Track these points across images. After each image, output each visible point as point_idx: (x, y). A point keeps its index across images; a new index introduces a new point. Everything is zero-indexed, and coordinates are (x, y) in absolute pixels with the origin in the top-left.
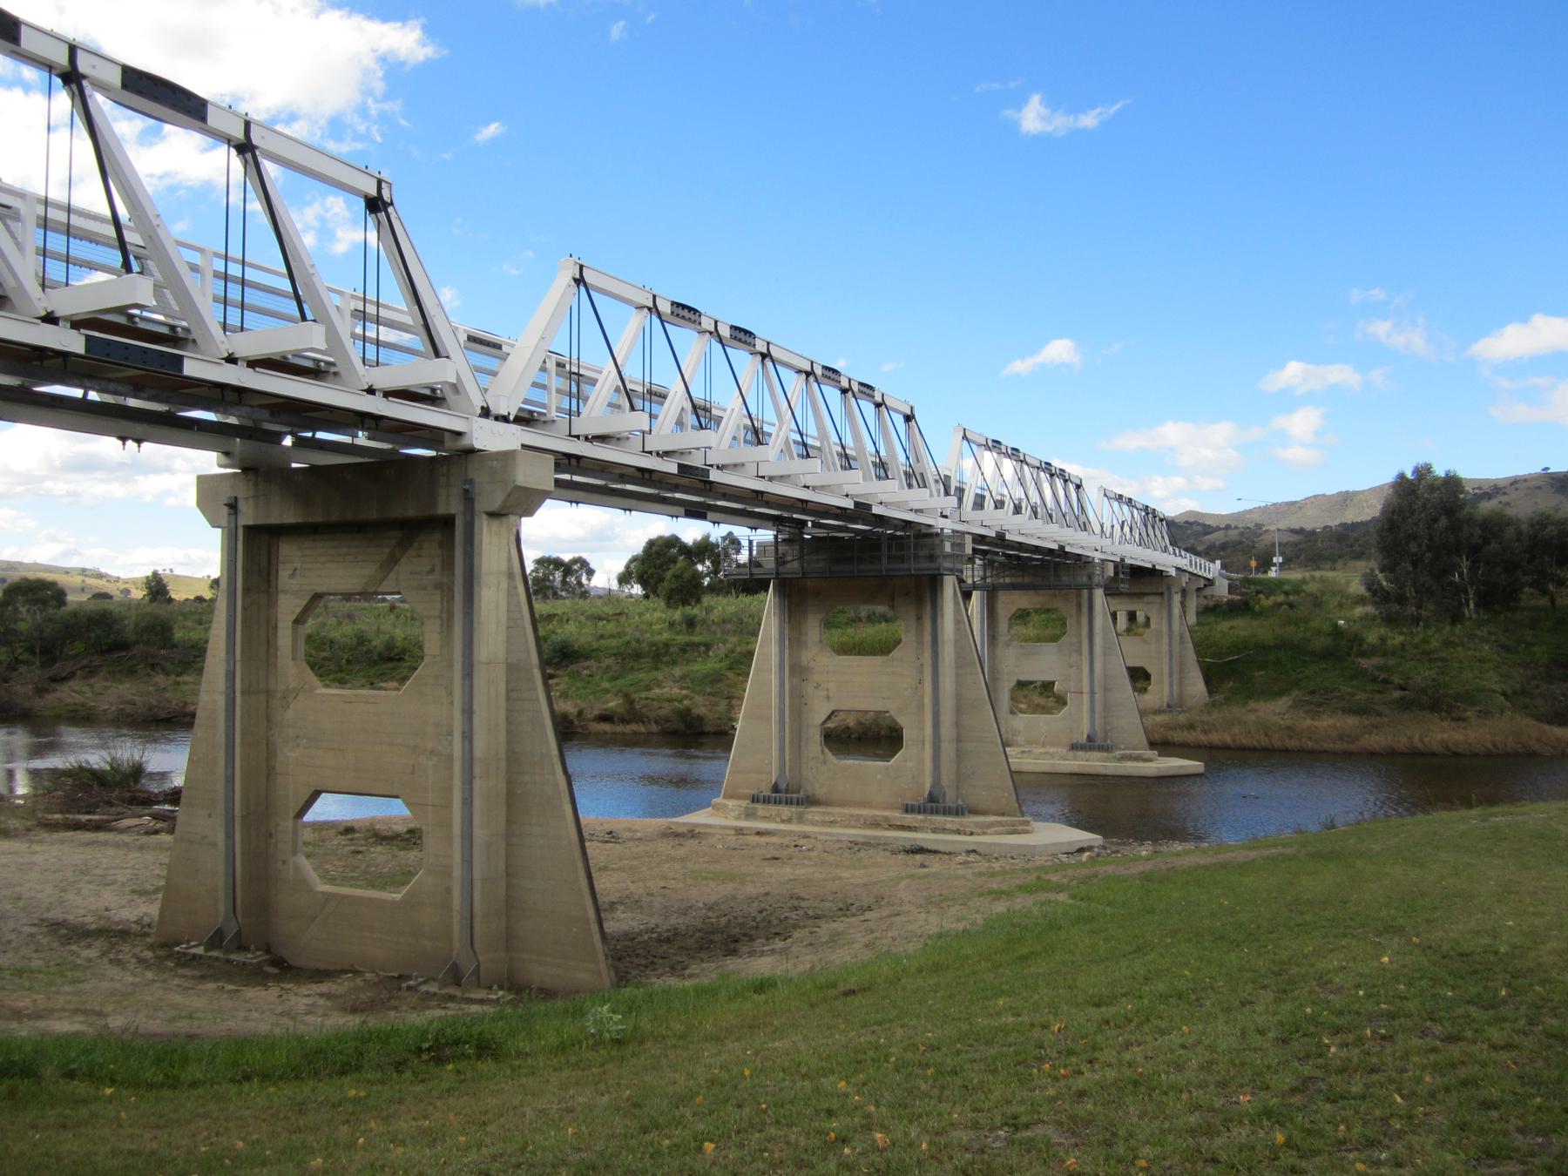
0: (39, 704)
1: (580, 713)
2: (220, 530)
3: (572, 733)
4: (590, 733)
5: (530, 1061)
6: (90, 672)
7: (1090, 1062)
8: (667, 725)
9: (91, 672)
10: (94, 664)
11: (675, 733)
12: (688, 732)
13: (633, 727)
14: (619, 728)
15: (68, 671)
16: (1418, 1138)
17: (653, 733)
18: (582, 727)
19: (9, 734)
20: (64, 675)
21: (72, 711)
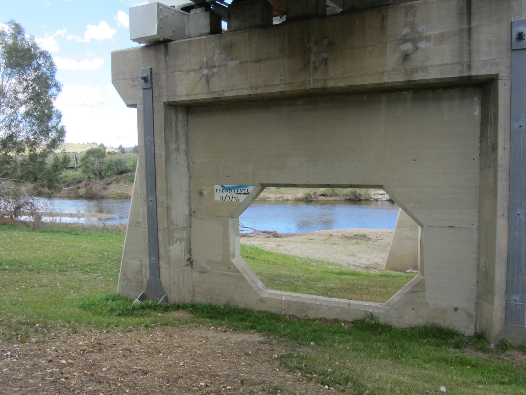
0: (105, 193)
1: (315, 193)
2: (327, 14)
3: (312, 200)
4: (319, 200)
5: (410, 387)
6: (118, 181)
7: (85, 231)
8: (346, 197)
9: (118, 182)
10: (119, 178)
11: (349, 200)
12: (356, 199)
13: (334, 198)
14: (330, 198)
15: (110, 181)
16: (299, 283)
17: (342, 200)
18: (315, 198)
19: (278, 188)
20: (109, 183)
21: (120, 196)
